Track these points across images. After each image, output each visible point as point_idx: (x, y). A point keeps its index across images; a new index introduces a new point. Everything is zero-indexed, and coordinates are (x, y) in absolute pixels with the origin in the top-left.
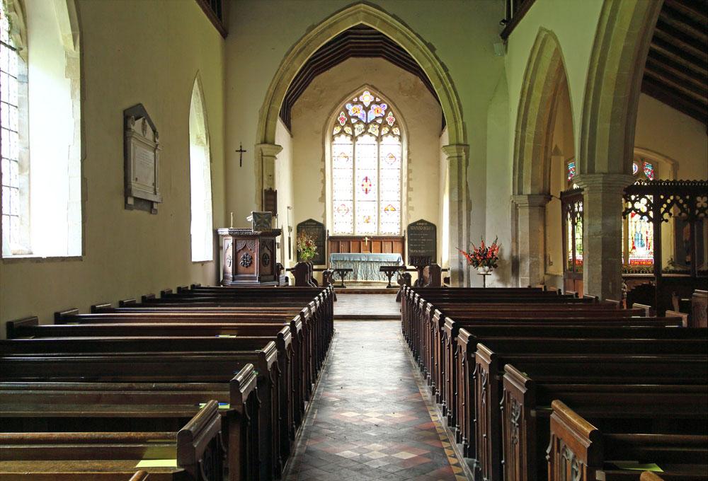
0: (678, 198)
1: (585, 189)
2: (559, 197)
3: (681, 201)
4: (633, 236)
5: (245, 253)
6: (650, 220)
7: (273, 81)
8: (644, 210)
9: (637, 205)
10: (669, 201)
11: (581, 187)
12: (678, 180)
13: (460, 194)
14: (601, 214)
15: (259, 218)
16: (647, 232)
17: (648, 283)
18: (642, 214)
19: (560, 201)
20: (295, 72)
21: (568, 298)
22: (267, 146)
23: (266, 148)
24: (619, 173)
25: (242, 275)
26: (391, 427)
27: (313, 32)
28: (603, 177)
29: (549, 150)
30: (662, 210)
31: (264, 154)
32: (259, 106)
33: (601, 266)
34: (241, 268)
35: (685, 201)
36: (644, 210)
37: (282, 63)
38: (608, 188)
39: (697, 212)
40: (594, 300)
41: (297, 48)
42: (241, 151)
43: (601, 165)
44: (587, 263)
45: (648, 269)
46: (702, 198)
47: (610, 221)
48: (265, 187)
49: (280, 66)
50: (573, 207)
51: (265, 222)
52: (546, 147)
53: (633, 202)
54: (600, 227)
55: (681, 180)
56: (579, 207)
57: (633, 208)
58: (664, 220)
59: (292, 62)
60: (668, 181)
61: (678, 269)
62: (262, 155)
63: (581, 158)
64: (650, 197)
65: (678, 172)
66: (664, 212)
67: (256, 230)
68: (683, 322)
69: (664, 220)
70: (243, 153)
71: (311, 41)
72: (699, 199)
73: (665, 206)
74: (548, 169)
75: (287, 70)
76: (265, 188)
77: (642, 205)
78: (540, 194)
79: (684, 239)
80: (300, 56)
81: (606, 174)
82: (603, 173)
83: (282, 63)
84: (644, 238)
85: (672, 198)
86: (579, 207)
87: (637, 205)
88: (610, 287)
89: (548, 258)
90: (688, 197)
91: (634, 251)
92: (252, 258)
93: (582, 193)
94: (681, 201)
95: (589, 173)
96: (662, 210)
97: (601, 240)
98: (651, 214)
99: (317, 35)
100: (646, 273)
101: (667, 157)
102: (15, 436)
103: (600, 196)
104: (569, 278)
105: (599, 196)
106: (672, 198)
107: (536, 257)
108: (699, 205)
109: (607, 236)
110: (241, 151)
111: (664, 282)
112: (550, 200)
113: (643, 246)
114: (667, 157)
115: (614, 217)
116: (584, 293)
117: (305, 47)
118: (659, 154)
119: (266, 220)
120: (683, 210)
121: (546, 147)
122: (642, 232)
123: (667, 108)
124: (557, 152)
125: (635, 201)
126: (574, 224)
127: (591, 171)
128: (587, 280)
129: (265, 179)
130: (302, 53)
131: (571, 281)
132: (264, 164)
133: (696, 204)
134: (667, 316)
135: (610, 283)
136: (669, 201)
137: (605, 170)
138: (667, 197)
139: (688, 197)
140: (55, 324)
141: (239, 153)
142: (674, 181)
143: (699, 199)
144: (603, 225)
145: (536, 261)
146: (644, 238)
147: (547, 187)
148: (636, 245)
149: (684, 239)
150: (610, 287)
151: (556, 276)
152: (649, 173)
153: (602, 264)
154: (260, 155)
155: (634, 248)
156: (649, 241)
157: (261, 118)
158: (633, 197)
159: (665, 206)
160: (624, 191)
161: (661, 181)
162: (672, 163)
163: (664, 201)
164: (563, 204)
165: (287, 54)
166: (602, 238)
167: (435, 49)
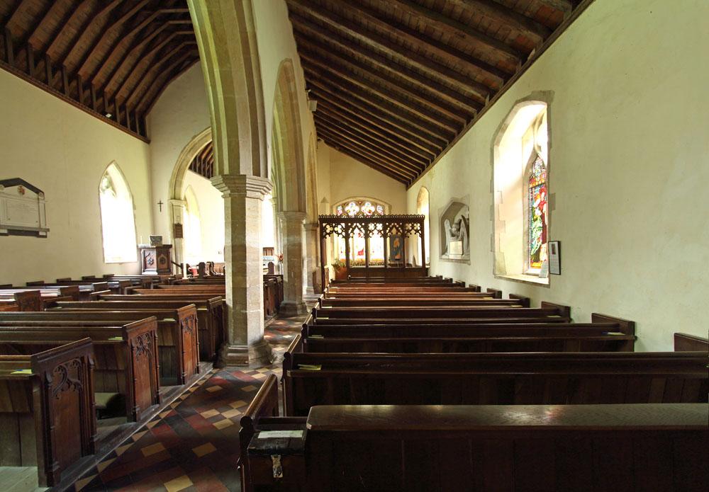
6: (343, 237)
9: (336, 229)
13: (277, 224)
18: (339, 234)
23: (174, 202)
30: (387, 231)
32: (169, 179)
34: (148, 266)
35: (400, 226)
53: (334, 227)
59: (186, 155)
64: (343, 225)
72: (407, 225)
75: (184, 160)
76: (175, 223)
80: (192, 151)
85: (393, 224)
87: (336, 229)
94: (360, 226)
96: (350, 231)
98: (344, 234)
99: (199, 141)
106: (393, 224)
108: (407, 229)
120: (398, 231)
125: (335, 227)
136: (391, 226)
138: (390, 224)
159: (351, 229)
163: (351, 226)
165: (182, 151)
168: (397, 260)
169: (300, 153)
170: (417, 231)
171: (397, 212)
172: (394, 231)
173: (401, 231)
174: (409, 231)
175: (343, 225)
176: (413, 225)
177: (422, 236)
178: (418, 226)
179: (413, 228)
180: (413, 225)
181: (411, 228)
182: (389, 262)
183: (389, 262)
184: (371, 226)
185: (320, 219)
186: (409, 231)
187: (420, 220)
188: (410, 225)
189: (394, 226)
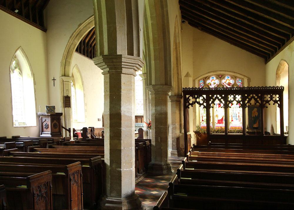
0: (218, 96)
4: (232, 114)
5: (46, 123)
6: (204, 107)
7: (65, 49)
8: (201, 102)
9: (198, 100)
12: (250, 87)
15: (49, 108)
16: (239, 113)
20: (76, 45)
22: (64, 77)
25: (45, 132)
26: (151, 190)
27: (82, 27)
30: (210, 102)
31: (64, 81)
32: (60, 60)
34: (45, 129)
35: (222, 98)
37: (69, 41)
39: (265, 102)
41: (75, 34)
42: (54, 80)
46: (239, 95)
48: (65, 95)
49: (68, 42)
51: (52, 110)
53: (196, 99)
55: (251, 87)
57: (196, 102)
58: (211, 107)
62: (63, 81)
64: (205, 96)
65: (250, 83)
66: (211, 103)
67: (48, 113)
69: (211, 107)
70: (55, 81)
71: (81, 31)
73: (212, 100)
78: (175, 95)
79: (253, 117)
83: (69, 41)
84: (237, 116)
85: (215, 96)
87: (198, 100)
88: (159, 139)
91: (232, 122)
92: (48, 125)
94: (220, 98)
96: (210, 102)
98: (205, 104)
99: (84, 27)
100: (234, 133)
102: (265, 165)
103: (154, 96)
106: (215, 96)
107: (175, 125)
110: (54, 80)
113: (237, 120)
115: (160, 106)
117: (79, 33)
119: (53, 109)
123: (248, 53)
125: (197, 98)
127: (151, 84)
129: (65, 91)
130: (78, 36)
132: (64, 85)
135: (159, 138)
136: (250, 97)
138: (248, 95)
141: (53, 81)
144: (155, 110)
145: (174, 127)
146: (237, 116)
148: (233, 119)
149: (253, 117)
150: (159, 139)
152: (240, 84)
154: (62, 81)
155: (232, 121)
157: (61, 65)
158: (196, 96)
159: (212, 100)
163: (212, 98)
166: (155, 116)
167: (81, 24)
170: (276, 102)
171: (256, 84)
172: (253, 102)
175: (205, 96)
177: (281, 106)
178: (277, 97)
184: (231, 98)
186: (231, 102)
187: (280, 91)
188: (269, 96)
189: (253, 97)
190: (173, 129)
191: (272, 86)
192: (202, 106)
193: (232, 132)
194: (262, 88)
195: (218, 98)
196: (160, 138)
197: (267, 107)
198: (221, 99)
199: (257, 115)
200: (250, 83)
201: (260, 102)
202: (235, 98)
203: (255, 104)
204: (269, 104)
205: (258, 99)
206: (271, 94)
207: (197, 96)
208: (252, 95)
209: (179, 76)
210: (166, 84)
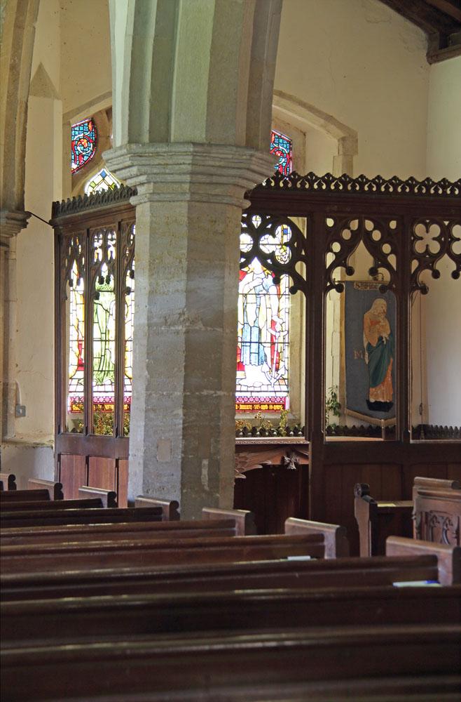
0: (369, 225)
1: (141, 190)
2: (49, 217)
3: (377, 236)
8: (283, 256)
10: (346, 235)
11: (129, 183)
14: (185, 263)
16: (273, 323)
17: (278, 463)
19: (51, 231)
21: (88, 511)
24: (237, 146)
28: (194, 154)
29: (23, 76)
30: (330, 258)
33: (180, 412)
35: (388, 236)
36: (283, 256)
38: (203, 188)
39: (415, 264)
40: (167, 512)
43: (189, 121)
44: (143, 406)
45: (276, 423)
46: (428, 226)
47: (207, 285)
50: (90, 251)
52: (14, 68)
54: (181, 302)
56: (105, 248)
57: (256, 252)
60: (328, 178)
61: (350, 423)
63: (131, 96)
64: (301, 223)
66: (334, 265)
68: (440, 568)
72: (419, 229)
73: (336, 247)
74: (18, 133)
77: (276, 244)
81: (202, 145)
82: (194, 144)
84: (266, 337)
85: (355, 225)
86: (105, 248)
88: (205, 472)
89: (12, 394)
90: (393, 225)
93: (133, 200)
94: (377, 236)
95: (152, 141)
96: (330, 258)
97: (183, 337)
98: (301, 268)
100: (271, 435)
101: (329, 119)
103: (185, 211)
104: (73, 452)
105: (181, 210)
106: (355, 225)
108: (419, 247)
109: (199, 326)
111: (331, 457)
112: (25, 225)
113: (261, 362)
114: (329, 119)
116: (133, 492)
118: (311, 109)
120: (381, 260)
121: (14, 68)
122: (261, 323)
124: (41, 85)
126: (91, 297)
127: (161, 135)
128: (141, 454)
131: (79, 461)
133: (412, 243)
134: (390, 553)
135: (205, 462)
136: (346, 235)
137: (200, 136)
138: (342, 224)
139: (393, 225)
140: (259, 534)
142: (345, 179)
143: (419, 229)
144: (189, 292)
147: (16, 189)
150: (205, 472)
151: (35, 446)
153: (186, 406)
156: (279, 347)
159: (336, 247)
160: (246, 197)
161: (311, 177)
162: (342, 134)
163: (335, 234)
164: (58, 238)
166: (187, 332)
168: (378, 406)
169: (62, 404)
172: (362, 258)
173: (392, 260)
174: (428, 261)
175: (301, 223)
176: (446, 232)
179: (446, 248)
180: (446, 232)
181: (435, 248)
182: (332, 419)
183: (332, 419)
184: (427, 237)
185: (245, 492)
186: (428, 261)
188: (435, 230)
189: (361, 234)
190: (152, 415)
191: (387, 179)
192: (286, 280)
193: (262, 433)
194: (379, 186)
195: (367, 236)
196: (210, 466)
197: (424, 290)
198: (382, 241)
199: (385, 335)
200: (356, 159)
201: (392, 260)
202: (446, 240)
203: (373, 272)
204: (436, 274)
205: (386, 248)
206: (446, 223)
207: (264, 222)
208: (356, 221)
209: (16, 89)
210: (250, 144)
